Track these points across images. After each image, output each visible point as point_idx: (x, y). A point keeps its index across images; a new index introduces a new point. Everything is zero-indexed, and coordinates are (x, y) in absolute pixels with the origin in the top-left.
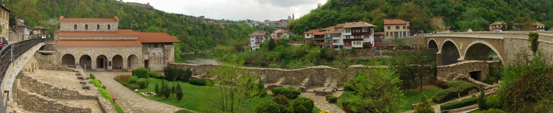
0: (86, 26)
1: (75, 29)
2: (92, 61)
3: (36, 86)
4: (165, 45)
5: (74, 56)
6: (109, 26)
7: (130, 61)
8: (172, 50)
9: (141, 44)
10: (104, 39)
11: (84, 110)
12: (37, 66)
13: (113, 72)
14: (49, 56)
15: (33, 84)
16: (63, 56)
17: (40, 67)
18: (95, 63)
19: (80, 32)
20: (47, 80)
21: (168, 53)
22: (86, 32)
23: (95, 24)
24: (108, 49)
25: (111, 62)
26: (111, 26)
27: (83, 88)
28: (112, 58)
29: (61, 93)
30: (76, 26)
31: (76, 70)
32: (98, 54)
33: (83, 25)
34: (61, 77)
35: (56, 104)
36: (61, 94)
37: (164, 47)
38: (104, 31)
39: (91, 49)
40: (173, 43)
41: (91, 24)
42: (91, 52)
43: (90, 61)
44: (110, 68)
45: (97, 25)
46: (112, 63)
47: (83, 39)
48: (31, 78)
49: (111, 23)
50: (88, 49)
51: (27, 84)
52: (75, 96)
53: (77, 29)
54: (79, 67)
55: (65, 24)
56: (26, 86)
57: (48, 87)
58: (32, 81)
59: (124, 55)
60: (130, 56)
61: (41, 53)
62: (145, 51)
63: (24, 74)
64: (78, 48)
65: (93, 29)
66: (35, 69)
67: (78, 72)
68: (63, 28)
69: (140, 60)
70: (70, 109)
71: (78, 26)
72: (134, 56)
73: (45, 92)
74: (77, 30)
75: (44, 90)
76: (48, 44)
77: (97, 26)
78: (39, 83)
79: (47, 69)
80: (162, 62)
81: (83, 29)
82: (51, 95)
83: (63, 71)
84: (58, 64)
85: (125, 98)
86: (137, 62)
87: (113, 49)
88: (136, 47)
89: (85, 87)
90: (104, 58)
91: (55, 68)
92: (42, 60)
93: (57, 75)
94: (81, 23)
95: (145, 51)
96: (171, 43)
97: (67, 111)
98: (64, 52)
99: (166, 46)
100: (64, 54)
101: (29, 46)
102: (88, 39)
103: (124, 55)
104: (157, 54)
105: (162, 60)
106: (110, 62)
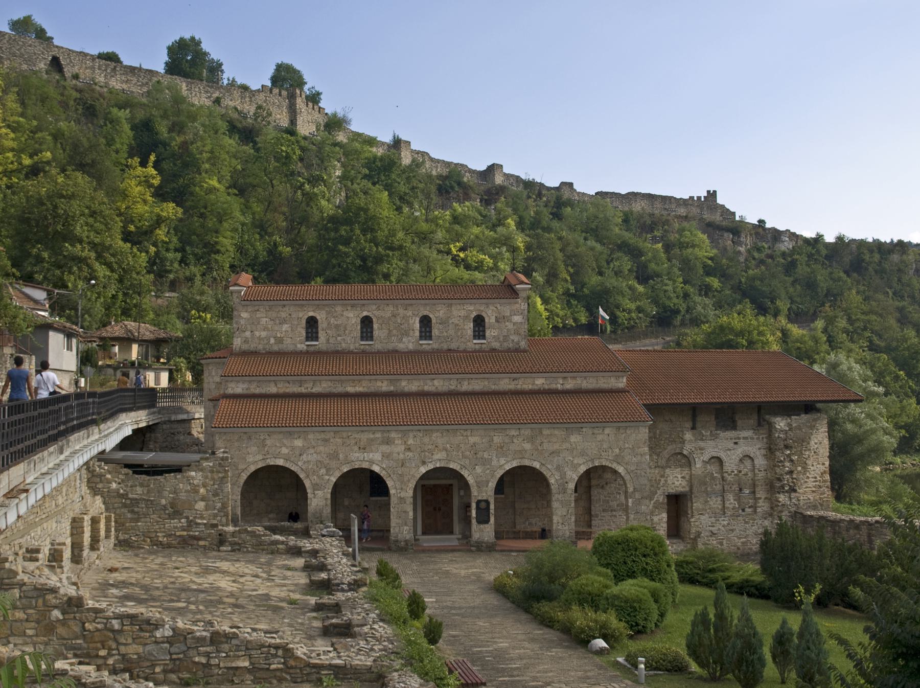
0: (367, 322)
1: (307, 339)
2: (394, 500)
3: (77, 629)
4: (776, 414)
5: (302, 476)
6: (479, 322)
7: (589, 500)
9: (645, 413)
10: (453, 385)
12: (102, 533)
13: (498, 555)
14: (171, 479)
16: (244, 476)
17: (121, 537)
18: (410, 509)
19: (338, 354)
20: (154, 599)
21: (795, 458)
22: (364, 352)
23: (410, 313)
24: (472, 440)
25: (487, 502)
26: (490, 319)
27: (327, 632)
28: (492, 485)
29: (207, 655)
30: (312, 323)
31: (306, 545)
32: (424, 463)
33: (353, 318)
34: (225, 583)
36: (204, 660)
37: (771, 426)
38: (453, 346)
39: (388, 442)
40: (819, 405)
41: (388, 311)
42: (387, 456)
43: (386, 498)
44: (484, 532)
45: (418, 320)
46: (492, 511)
47: (350, 389)
48: (54, 591)
49: (487, 305)
52: (273, 667)
53: (317, 339)
54: (324, 532)
56: (30, 632)
57: (141, 630)
58: (56, 607)
59: (558, 468)
60: (588, 473)
61: (127, 466)
62: (671, 448)
63: (16, 573)
64: (323, 436)
65: (400, 341)
67: (314, 553)
68: (248, 334)
69: (637, 496)
71: (322, 325)
72: (608, 476)
73: (124, 656)
74: (321, 343)
76: (173, 418)
77: (417, 325)
78: (97, 611)
81: (351, 340)
82: (158, 670)
83: (238, 555)
84: (215, 516)
85: (535, 679)
86: (627, 506)
87: (497, 439)
88: (619, 428)
89: (335, 626)
90: (454, 482)
91: (198, 539)
92: (136, 502)
93: (206, 571)
94: (339, 309)
95: (671, 448)
96: (808, 408)
98: (250, 459)
99: (781, 423)
100: (253, 468)
101: (44, 432)
102: (372, 389)
103: (558, 468)
104: (731, 464)
105: (761, 494)
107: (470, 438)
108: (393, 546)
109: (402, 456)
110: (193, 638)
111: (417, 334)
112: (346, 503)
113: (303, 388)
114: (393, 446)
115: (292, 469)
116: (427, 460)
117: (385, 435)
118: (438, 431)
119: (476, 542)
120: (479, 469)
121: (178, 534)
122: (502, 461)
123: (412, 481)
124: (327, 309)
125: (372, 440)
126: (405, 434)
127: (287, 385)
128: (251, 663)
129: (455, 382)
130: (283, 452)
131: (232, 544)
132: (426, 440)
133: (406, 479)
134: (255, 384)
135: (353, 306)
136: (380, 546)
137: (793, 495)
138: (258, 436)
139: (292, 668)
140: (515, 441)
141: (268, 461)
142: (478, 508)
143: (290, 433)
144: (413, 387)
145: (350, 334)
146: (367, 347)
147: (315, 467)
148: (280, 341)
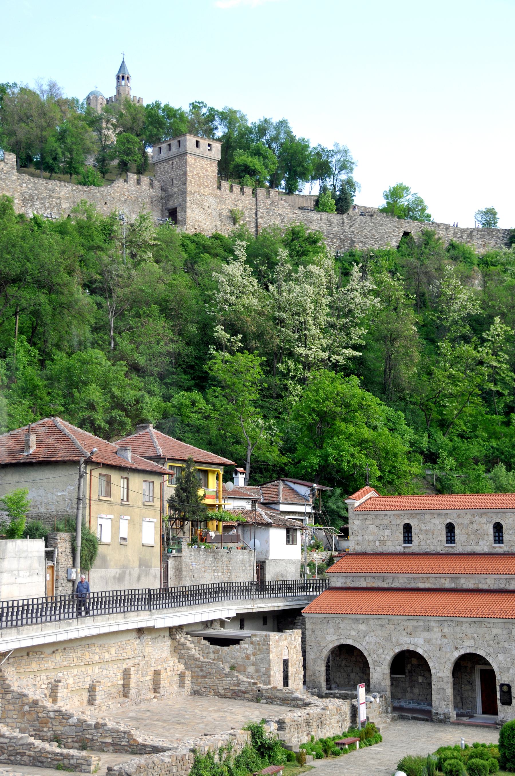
5: (366, 654)
11: (77, 759)
15: (29, 712)
24: (495, 631)
32: (457, 648)
35: (24, 744)
39: (428, 629)
42: (428, 641)
45: (491, 526)
47: (421, 586)
50: (416, 628)
51: (17, 713)
52: (123, 743)
55: (367, 522)
64: (380, 622)
65: (477, 543)
70: (50, 756)
75: (54, 727)
77: (491, 531)
79: (217, 694)
82: (70, 740)
91: (244, 692)
97: (45, 760)
98: (329, 638)
100: (331, 646)
106: (505, 689)
107: (493, 630)
108: (434, 717)
109: (439, 642)
110: (86, 724)
111: (492, 538)
112: (420, 680)
113: (385, 583)
114: (432, 633)
115: (359, 648)
116: (459, 646)
117: (426, 623)
118: (467, 622)
119: (501, 721)
120: (501, 657)
121: (231, 688)
123: (448, 663)
124: (418, 517)
125: (416, 627)
126: (441, 623)
127: (374, 580)
128: (113, 741)
129: (504, 581)
130: (352, 634)
131: (267, 698)
132: (458, 629)
133: (443, 661)
134: (351, 579)
135: (439, 515)
136: (425, 717)
138: (334, 621)
139: (131, 745)
141: (342, 640)
142: (501, 691)
143: (357, 619)
144: (470, 585)
145: (436, 538)
146: (451, 549)
147: (375, 647)
148: (383, 543)
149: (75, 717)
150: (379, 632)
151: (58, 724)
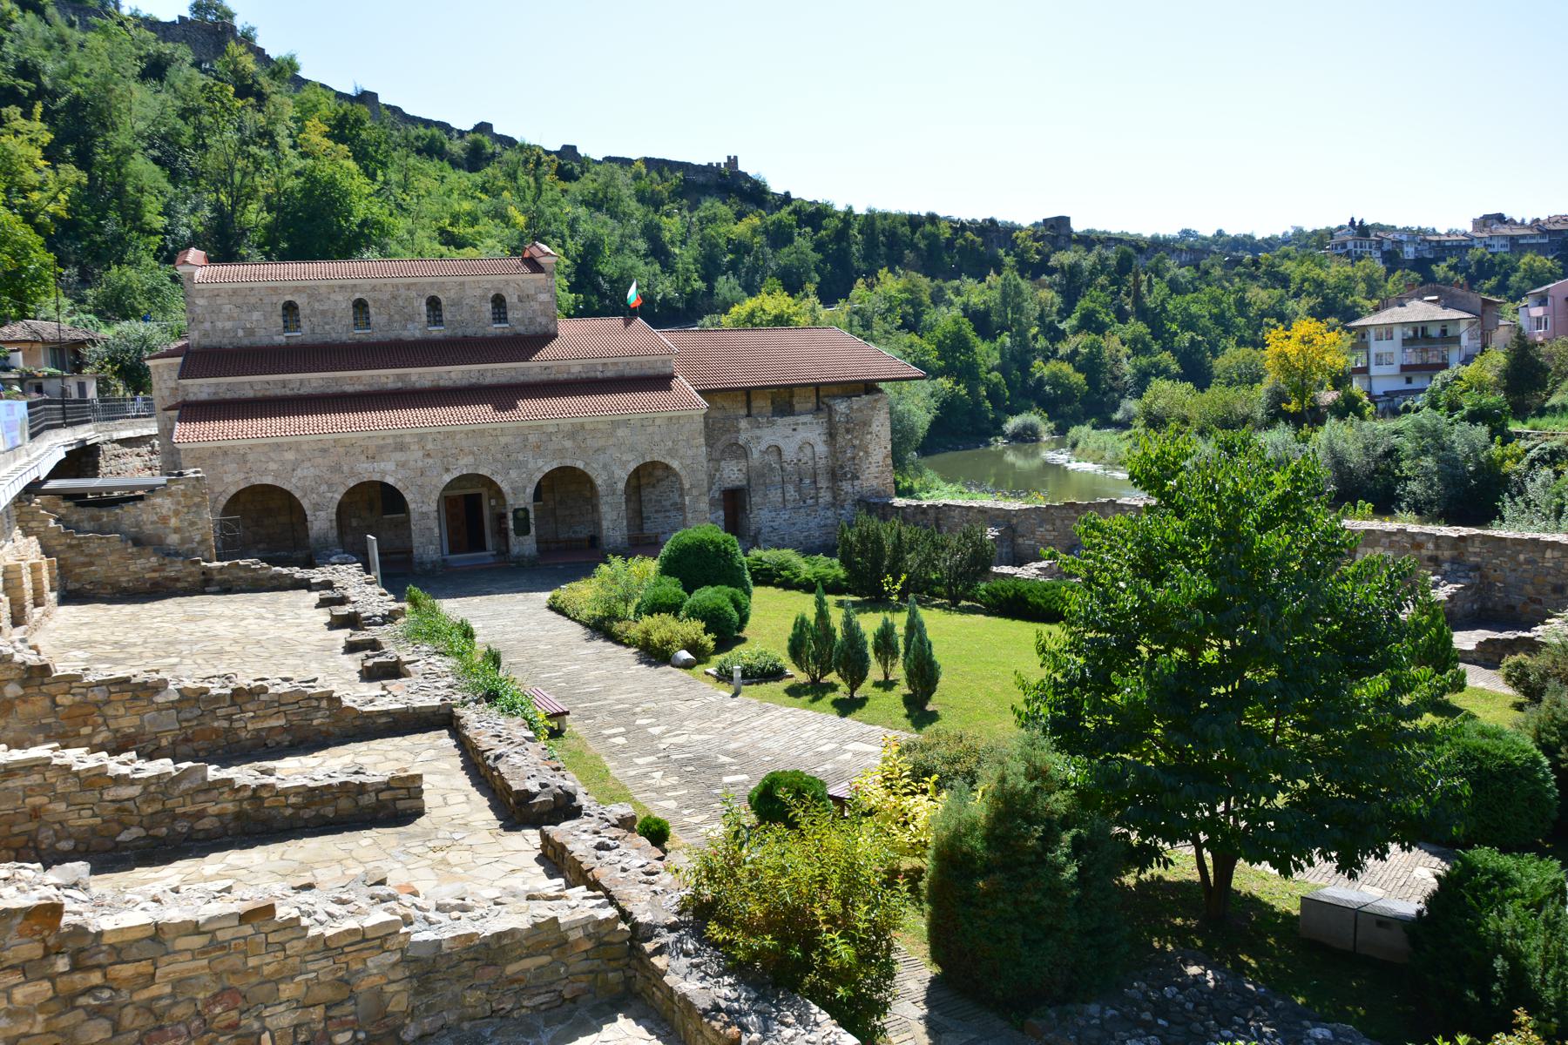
8: (874, 428)
27: (369, 675)
28: (530, 490)
32: (447, 470)
45: (424, 302)
65: (405, 328)
66: (36, 605)
77: (424, 308)
80: (825, 497)
99: (841, 407)
100: (233, 490)
103: (605, 467)
105: (823, 483)
109: (420, 464)
111: (425, 318)
120: (513, 474)
122: (540, 463)
137: (856, 483)
140: (554, 438)
149: (171, 687)
150: (320, 460)
151: (122, 711)
